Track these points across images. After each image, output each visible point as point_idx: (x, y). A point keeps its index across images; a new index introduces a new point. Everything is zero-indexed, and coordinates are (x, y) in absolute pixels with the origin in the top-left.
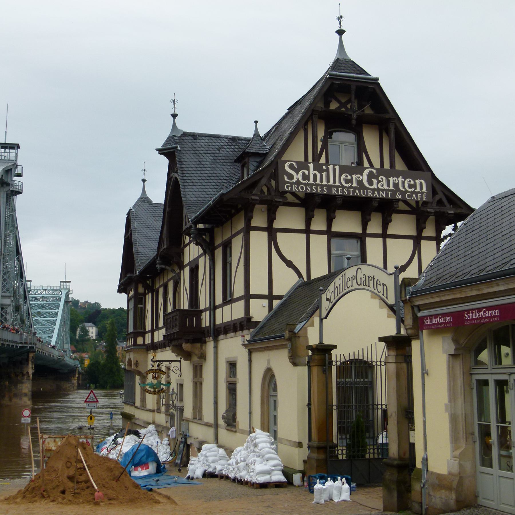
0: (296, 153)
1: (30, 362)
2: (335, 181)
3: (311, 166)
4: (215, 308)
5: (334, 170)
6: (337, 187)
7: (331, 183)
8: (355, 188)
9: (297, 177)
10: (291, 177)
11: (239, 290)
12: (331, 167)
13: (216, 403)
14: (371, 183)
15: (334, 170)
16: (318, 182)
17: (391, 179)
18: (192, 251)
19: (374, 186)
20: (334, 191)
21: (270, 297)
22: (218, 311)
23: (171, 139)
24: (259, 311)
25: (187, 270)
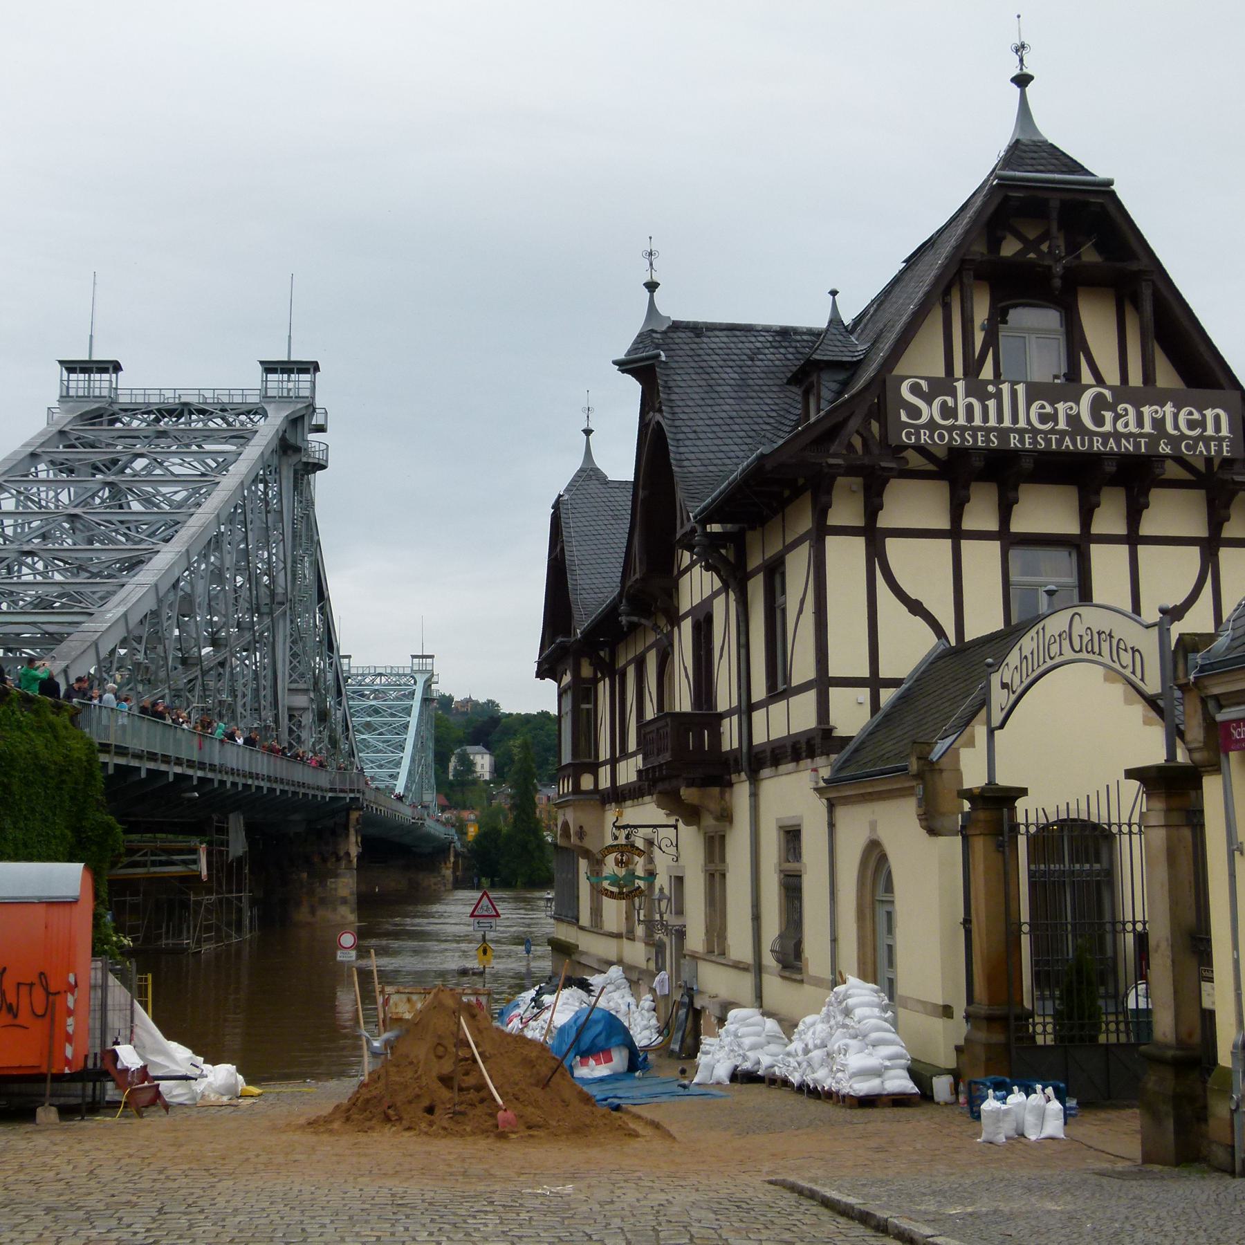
0: (926, 359)
1: (352, 831)
2: (1015, 419)
5: (1014, 394)
6: (1021, 432)
7: (1007, 423)
8: (1063, 433)
10: (915, 412)
11: (802, 668)
13: (756, 918)
14: (1099, 421)
15: (1014, 394)
16: (978, 422)
17: (1146, 410)
18: (697, 584)
19: (1108, 427)
20: (1014, 441)
21: (874, 682)
24: (850, 714)
25: (687, 626)
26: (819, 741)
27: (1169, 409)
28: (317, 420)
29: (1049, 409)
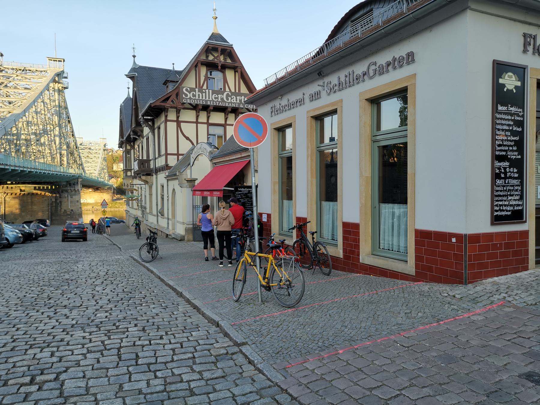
0: (190, 82)
1: (79, 184)
2: (209, 98)
3: (197, 90)
4: (155, 159)
5: (209, 92)
6: (210, 101)
7: (207, 99)
8: (220, 102)
9: (190, 95)
10: (186, 95)
11: (163, 152)
12: (207, 91)
13: (157, 205)
14: (228, 99)
15: (209, 92)
16: (201, 98)
17: (238, 97)
18: (146, 130)
19: (229, 101)
20: (209, 103)
21: (178, 155)
22: (157, 160)
23: (133, 70)
24: (172, 161)
25: (145, 138)
26: (167, 167)
27: (243, 97)
28: (65, 75)
29: (217, 96)
